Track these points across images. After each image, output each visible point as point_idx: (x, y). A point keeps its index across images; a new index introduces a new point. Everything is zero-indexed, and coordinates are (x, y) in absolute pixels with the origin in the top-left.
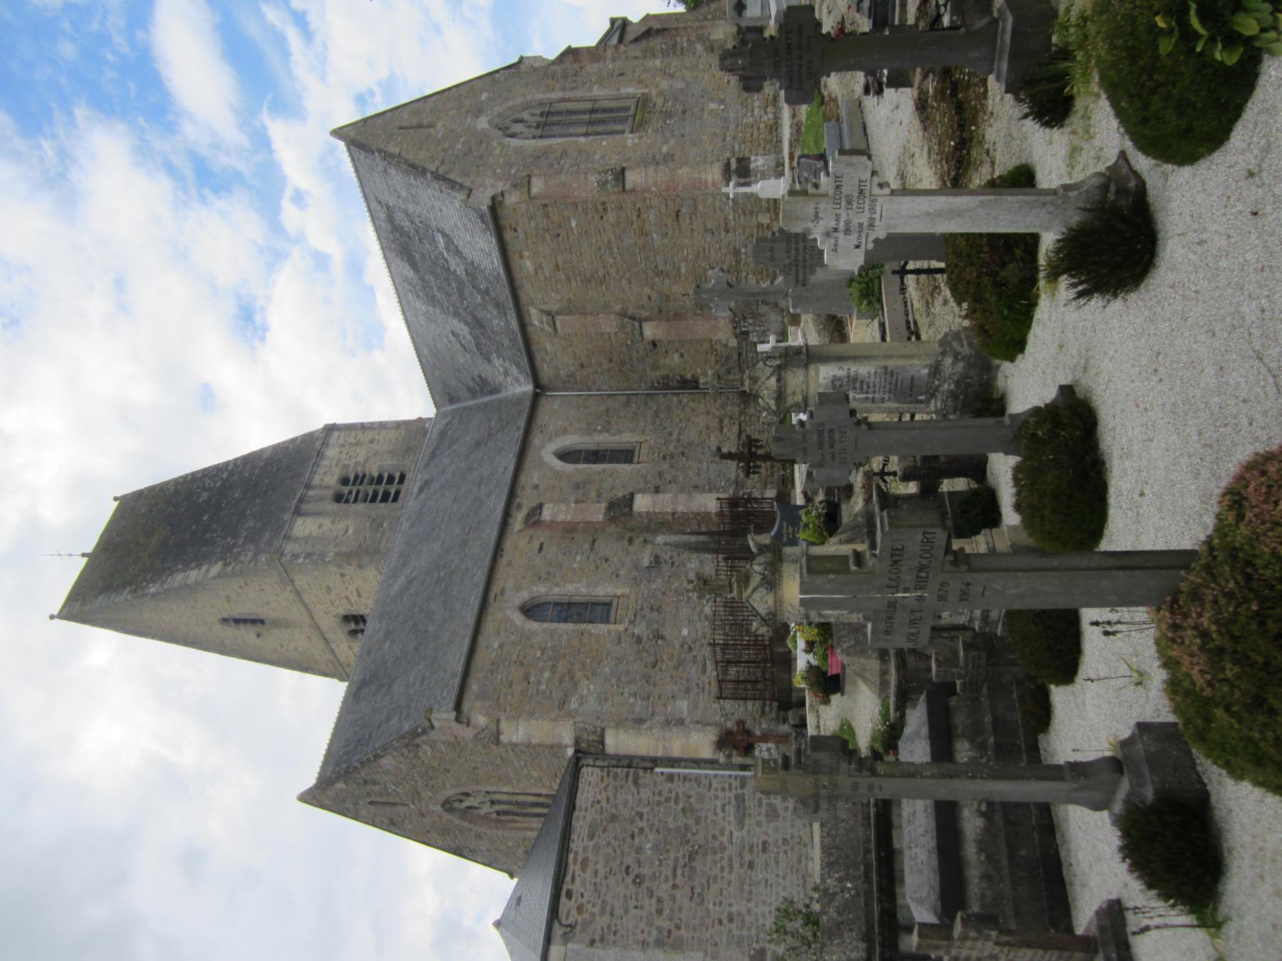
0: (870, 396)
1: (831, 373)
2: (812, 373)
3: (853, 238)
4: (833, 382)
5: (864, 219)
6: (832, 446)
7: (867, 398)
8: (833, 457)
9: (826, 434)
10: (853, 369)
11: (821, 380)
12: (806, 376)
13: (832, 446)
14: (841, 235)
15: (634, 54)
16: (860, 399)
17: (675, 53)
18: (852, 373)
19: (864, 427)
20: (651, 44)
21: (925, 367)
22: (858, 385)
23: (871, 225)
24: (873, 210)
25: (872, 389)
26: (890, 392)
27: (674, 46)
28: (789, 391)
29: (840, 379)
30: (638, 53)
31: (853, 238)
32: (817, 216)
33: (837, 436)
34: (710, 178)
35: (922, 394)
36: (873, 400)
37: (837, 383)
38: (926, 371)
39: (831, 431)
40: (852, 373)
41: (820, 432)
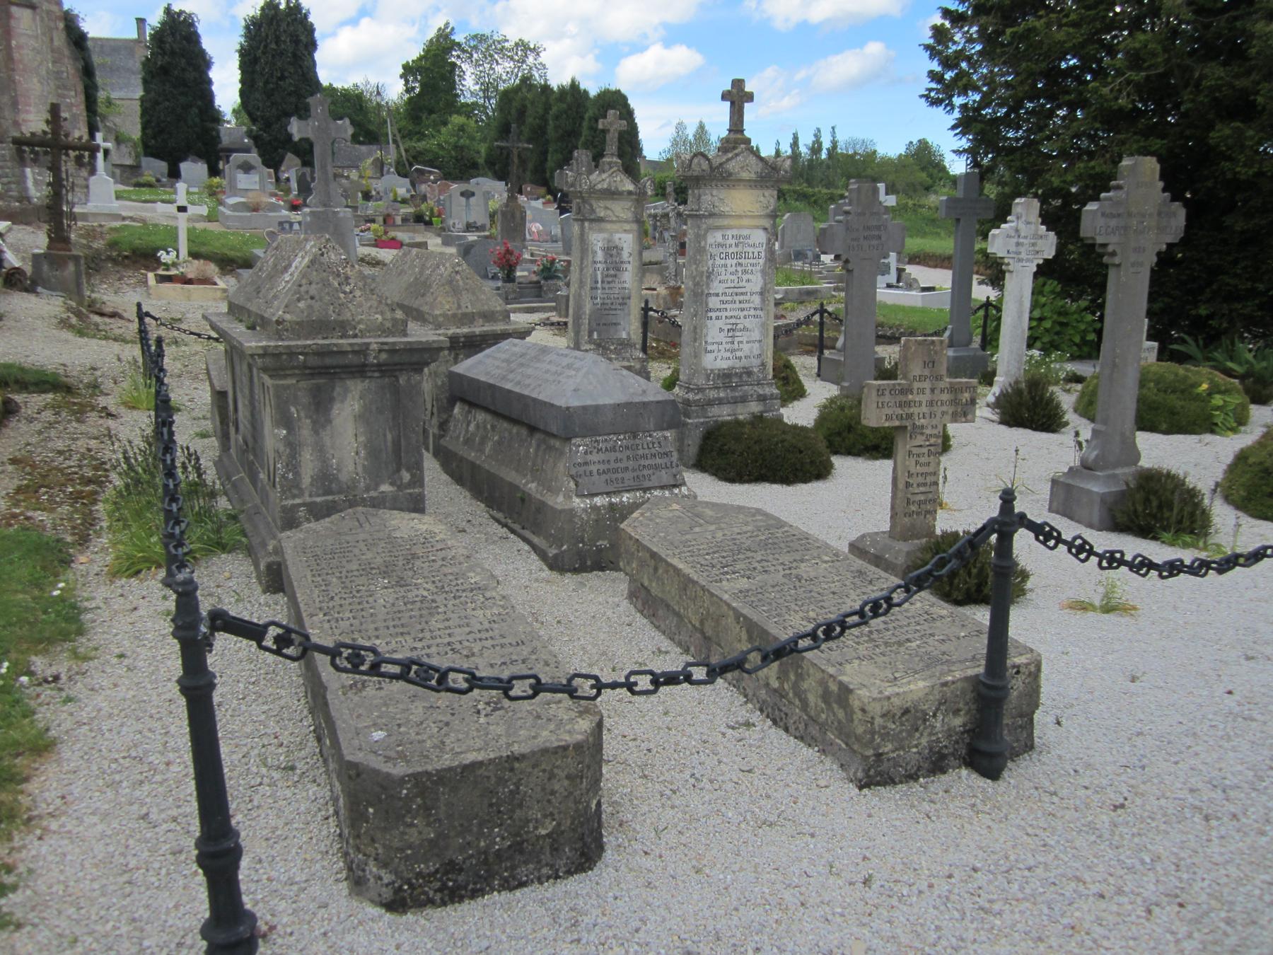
0: (599, 285)
1: (625, 246)
2: (627, 227)
3: (1013, 249)
4: (616, 247)
5: (1023, 256)
6: (865, 238)
7: (596, 282)
8: (857, 239)
9: (876, 233)
10: (630, 267)
11: (617, 236)
12: (626, 221)
13: (865, 238)
14: (1015, 240)
15: (56, 39)
16: (596, 276)
17: (58, 87)
18: (625, 266)
19: (850, 266)
20: (66, 60)
21: (629, 334)
22: (612, 272)
23: (1020, 260)
24: (1028, 260)
25: (606, 286)
26: (603, 304)
27: (65, 87)
28: (609, 204)
29: (619, 254)
30: (56, 43)
31: (1013, 249)
32: (1028, 223)
33: (875, 242)
34: (31, 117)
35: (599, 335)
36: (594, 289)
37: (614, 252)
38: (624, 335)
39: (879, 237)
40: (625, 266)
41: (878, 228)
